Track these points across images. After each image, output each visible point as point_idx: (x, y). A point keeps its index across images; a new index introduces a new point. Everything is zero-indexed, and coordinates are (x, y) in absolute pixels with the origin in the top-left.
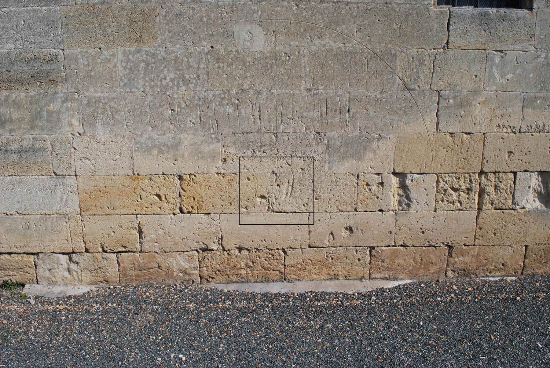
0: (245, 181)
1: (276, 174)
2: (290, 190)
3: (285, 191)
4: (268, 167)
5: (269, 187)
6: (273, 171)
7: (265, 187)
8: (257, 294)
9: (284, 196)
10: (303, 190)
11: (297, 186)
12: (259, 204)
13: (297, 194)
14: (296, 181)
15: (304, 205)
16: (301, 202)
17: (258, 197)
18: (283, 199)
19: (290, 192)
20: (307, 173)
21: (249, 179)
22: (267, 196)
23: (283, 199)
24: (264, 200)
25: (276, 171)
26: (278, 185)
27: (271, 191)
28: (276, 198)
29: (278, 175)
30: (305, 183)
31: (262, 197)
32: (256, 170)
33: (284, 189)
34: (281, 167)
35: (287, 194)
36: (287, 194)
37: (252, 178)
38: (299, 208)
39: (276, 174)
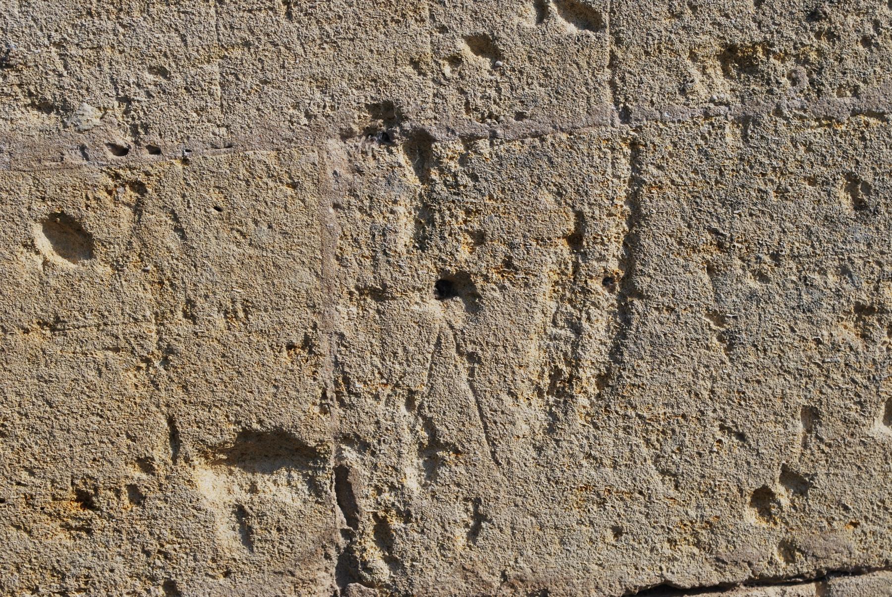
0: (27, 265)
1: (421, 147)
2: (599, 328)
3: (533, 352)
4: (323, 61)
5: (344, 315)
6: (388, 112)
7: (296, 322)
8: (632, 176)
9: (529, 414)
10: (750, 325)
11: (680, 278)
12: (226, 534)
13: (680, 372)
14: (666, 213)
15: (763, 499)
16: (727, 464)
17: (212, 454)
18: (520, 451)
19: (594, 353)
20: (792, 99)
21: (70, 235)
22: (319, 427)
23: (520, 451)
24: (282, 491)
25: (419, 112)
26: (448, 287)
27: (365, 368)
28: (432, 453)
29: (449, 148)
30: (770, 233)
31: (262, 449)
32: (162, 114)
33: (528, 326)
34: (485, 45)
35: (560, 387)
36: (560, 387)
37: (112, 222)
38: (705, 535)
39: (421, 147)
